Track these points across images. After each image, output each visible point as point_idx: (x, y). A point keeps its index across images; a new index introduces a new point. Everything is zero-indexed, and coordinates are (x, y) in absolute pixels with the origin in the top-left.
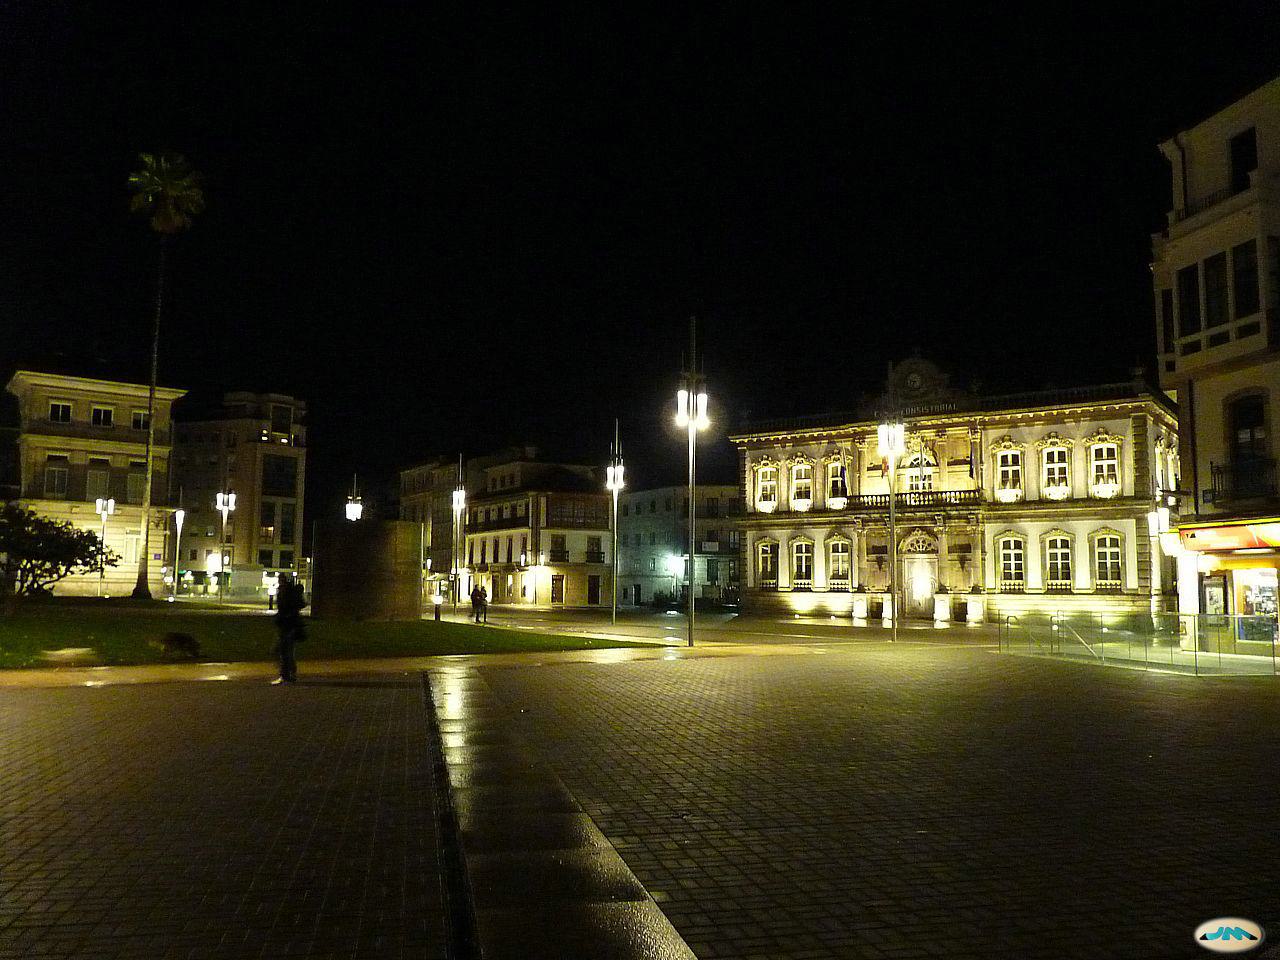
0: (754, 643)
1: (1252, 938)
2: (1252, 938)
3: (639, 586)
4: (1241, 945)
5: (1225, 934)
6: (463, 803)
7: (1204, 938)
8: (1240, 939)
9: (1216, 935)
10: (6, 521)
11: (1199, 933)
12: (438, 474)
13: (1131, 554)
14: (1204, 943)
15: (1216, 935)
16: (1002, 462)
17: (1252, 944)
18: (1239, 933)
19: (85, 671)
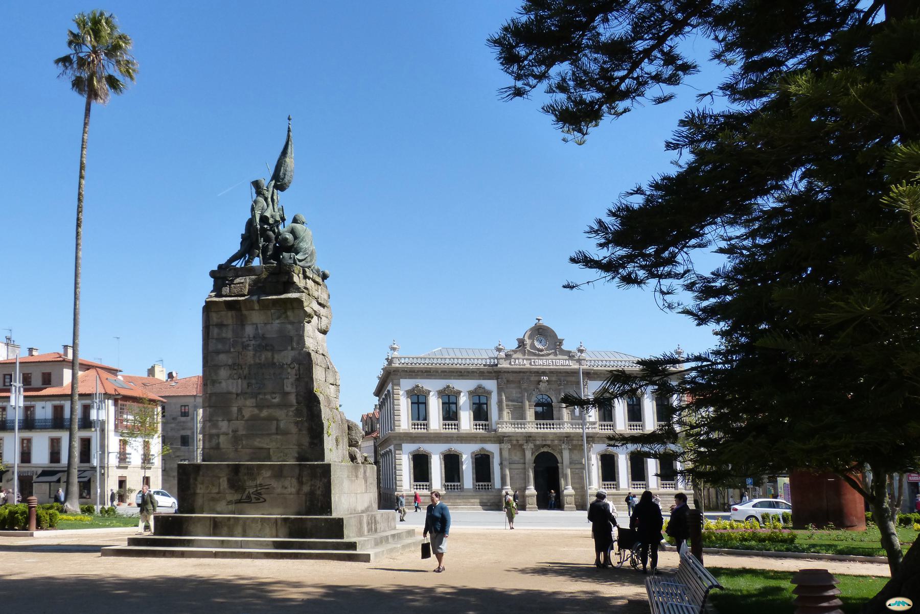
0: (86, 400)
1: (909, 605)
2: (909, 605)
3: (164, 406)
4: (906, 608)
5: (898, 604)
6: (468, 613)
7: (890, 605)
8: (904, 605)
9: (894, 604)
10: (219, 195)
11: (888, 603)
12: (679, 506)
13: (867, 569)
14: (890, 607)
15: (894, 604)
16: (185, 416)
17: (909, 607)
18: (903, 603)
19: (34, 575)
